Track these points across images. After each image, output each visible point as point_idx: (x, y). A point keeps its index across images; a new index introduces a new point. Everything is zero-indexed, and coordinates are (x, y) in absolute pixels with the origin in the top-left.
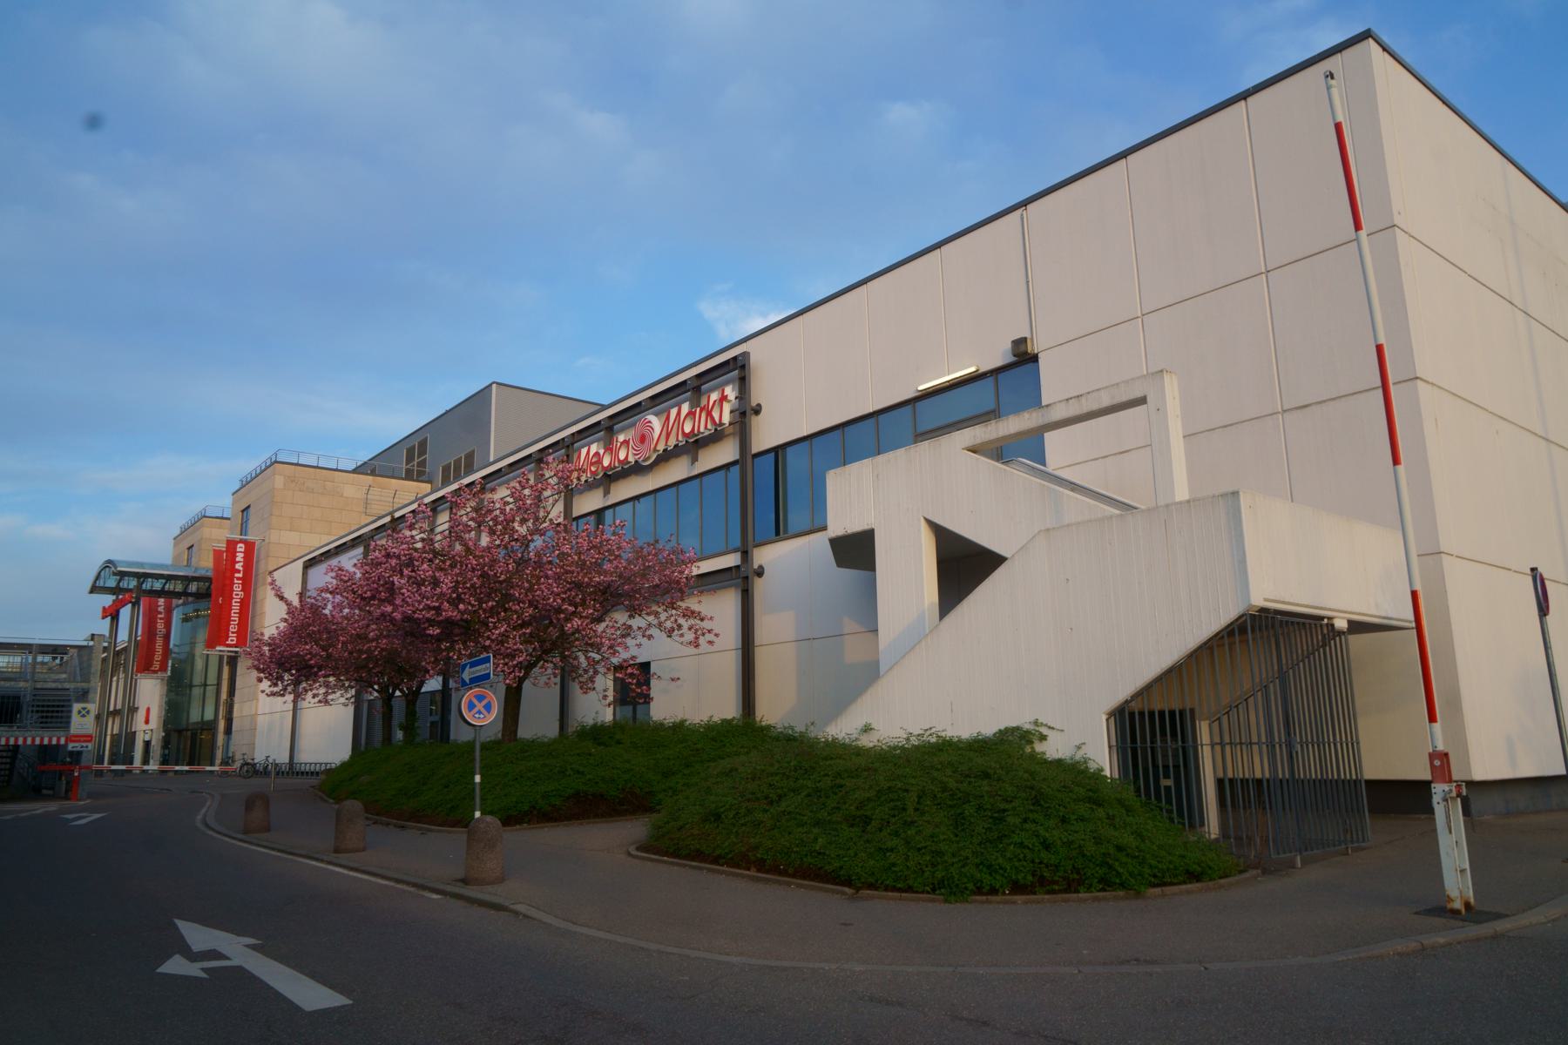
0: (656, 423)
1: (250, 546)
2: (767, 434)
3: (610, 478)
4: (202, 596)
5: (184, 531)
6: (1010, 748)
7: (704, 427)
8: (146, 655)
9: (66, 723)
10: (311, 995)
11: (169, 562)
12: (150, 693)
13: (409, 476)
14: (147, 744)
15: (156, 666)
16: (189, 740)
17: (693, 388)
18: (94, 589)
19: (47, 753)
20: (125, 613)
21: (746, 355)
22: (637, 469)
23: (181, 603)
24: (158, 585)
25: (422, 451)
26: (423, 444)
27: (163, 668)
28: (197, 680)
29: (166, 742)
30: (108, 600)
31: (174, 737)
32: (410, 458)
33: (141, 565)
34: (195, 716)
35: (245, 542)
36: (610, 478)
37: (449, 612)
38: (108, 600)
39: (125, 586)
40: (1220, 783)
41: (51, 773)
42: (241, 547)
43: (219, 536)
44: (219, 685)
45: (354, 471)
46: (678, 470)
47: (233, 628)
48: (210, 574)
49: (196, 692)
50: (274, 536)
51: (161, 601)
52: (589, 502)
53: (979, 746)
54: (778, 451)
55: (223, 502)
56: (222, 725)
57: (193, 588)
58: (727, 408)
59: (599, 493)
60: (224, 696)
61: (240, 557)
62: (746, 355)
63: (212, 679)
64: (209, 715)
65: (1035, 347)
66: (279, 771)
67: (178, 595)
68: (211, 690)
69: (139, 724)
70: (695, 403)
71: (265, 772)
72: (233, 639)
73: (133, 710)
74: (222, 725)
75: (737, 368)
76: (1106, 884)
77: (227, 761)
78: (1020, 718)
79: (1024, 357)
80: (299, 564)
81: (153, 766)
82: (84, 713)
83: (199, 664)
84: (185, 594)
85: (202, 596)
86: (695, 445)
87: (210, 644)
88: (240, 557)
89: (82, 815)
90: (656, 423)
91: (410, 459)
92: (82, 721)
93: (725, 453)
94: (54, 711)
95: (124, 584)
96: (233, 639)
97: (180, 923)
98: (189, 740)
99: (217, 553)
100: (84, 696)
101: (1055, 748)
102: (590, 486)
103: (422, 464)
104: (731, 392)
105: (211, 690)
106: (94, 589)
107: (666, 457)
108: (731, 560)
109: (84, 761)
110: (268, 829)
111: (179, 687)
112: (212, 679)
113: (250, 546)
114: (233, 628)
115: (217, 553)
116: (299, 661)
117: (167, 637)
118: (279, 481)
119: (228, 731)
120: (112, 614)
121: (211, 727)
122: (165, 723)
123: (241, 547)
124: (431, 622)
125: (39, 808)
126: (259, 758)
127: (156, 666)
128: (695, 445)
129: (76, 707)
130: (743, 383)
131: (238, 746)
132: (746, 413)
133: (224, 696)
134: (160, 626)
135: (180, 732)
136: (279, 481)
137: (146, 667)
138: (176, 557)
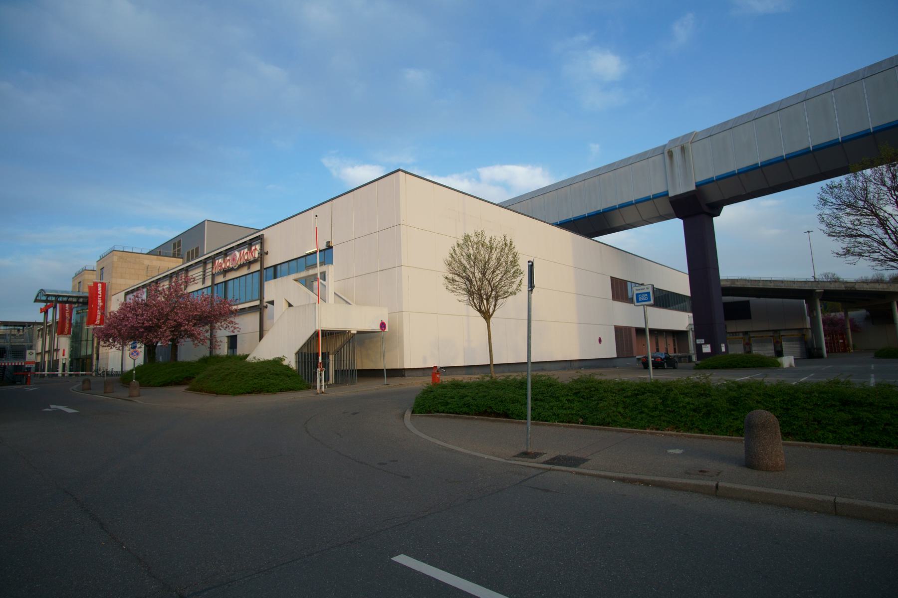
0: (237, 253)
1: (104, 285)
2: (270, 261)
3: (226, 271)
4: (85, 303)
5: (102, 258)
6: (278, 362)
7: (251, 258)
8: (61, 328)
9: (24, 357)
10: (402, 559)
11: (70, 289)
12: (64, 343)
13: (174, 256)
14: (64, 364)
15: (66, 332)
16: (81, 362)
17: (250, 244)
18: (36, 301)
19: (17, 368)
20: (51, 311)
21: (263, 235)
22: (232, 270)
23: (76, 308)
24: (65, 299)
25: (179, 245)
26: (179, 242)
27: (69, 333)
28: (84, 337)
29: (71, 364)
30: (43, 305)
31: (75, 362)
32: (174, 248)
33: (57, 291)
34: (83, 353)
35: (102, 283)
36: (226, 271)
37: (147, 324)
38: (43, 305)
39: (48, 300)
40: (335, 371)
41: (20, 375)
42: (100, 285)
43: (91, 279)
44: (93, 340)
45: (148, 254)
46: (244, 271)
47: (99, 317)
48: (87, 295)
49: (84, 343)
50: (114, 281)
51: (67, 305)
52: (220, 279)
53: (268, 362)
54: (275, 267)
55: (93, 264)
56: (95, 356)
57: (81, 300)
58: (257, 252)
59: (246, 268)
60: (95, 345)
61: (100, 289)
62: (263, 235)
63: (90, 338)
64: (89, 352)
65: (333, 244)
66: (117, 374)
67: (75, 303)
68: (90, 343)
69: (60, 356)
70: (250, 249)
71: (112, 375)
72: (98, 322)
73: (57, 350)
74: (95, 356)
75: (260, 239)
76: (268, 392)
77: (97, 371)
78: (280, 356)
79: (329, 247)
80: (123, 294)
81: (67, 372)
82: (31, 354)
83: (85, 331)
84: (78, 302)
85: (85, 303)
86: (249, 263)
87: (89, 324)
88: (100, 289)
89: (30, 388)
90: (237, 253)
91: (174, 248)
92: (31, 357)
93: (256, 267)
94: (19, 353)
95: (50, 299)
96: (98, 322)
97: (395, 559)
98: (81, 362)
99: (90, 287)
100: (31, 348)
101: (285, 363)
102: (219, 274)
103: (179, 250)
104: (258, 247)
105: (90, 343)
106: (36, 301)
107: (241, 266)
108: (257, 303)
109: (33, 370)
110: (90, 389)
111: (76, 341)
112: (90, 338)
113: (104, 285)
114: (99, 317)
115: (90, 287)
116: (121, 330)
117: (70, 320)
118: (115, 258)
119: (98, 359)
120: (45, 311)
121: (91, 357)
122: (71, 356)
123: (100, 285)
124: (141, 327)
125: (15, 387)
126: (109, 369)
127: (66, 332)
128: (249, 263)
129: (28, 352)
130: (262, 244)
131: (102, 365)
132: (263, 253)
133: (95, 345)
134: (67, 315)
135: (77, 359)
136: (115, 258)
137: (61, 332)
138: (74, 287)
